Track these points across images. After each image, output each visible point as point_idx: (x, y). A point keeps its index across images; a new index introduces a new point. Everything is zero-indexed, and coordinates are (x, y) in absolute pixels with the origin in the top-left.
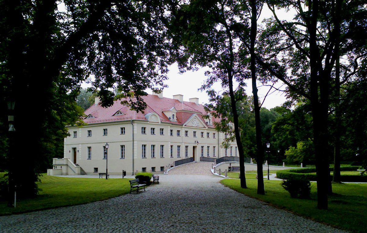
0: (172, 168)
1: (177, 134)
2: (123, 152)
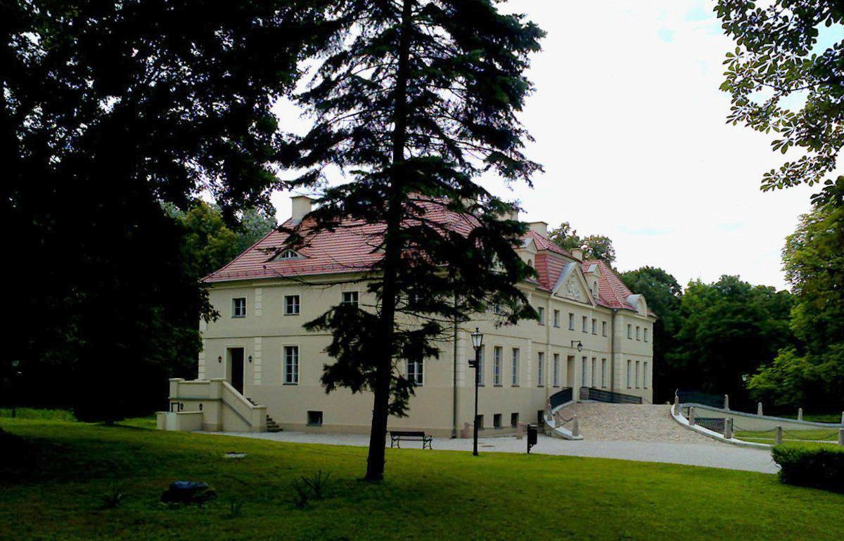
2: (293, 364)
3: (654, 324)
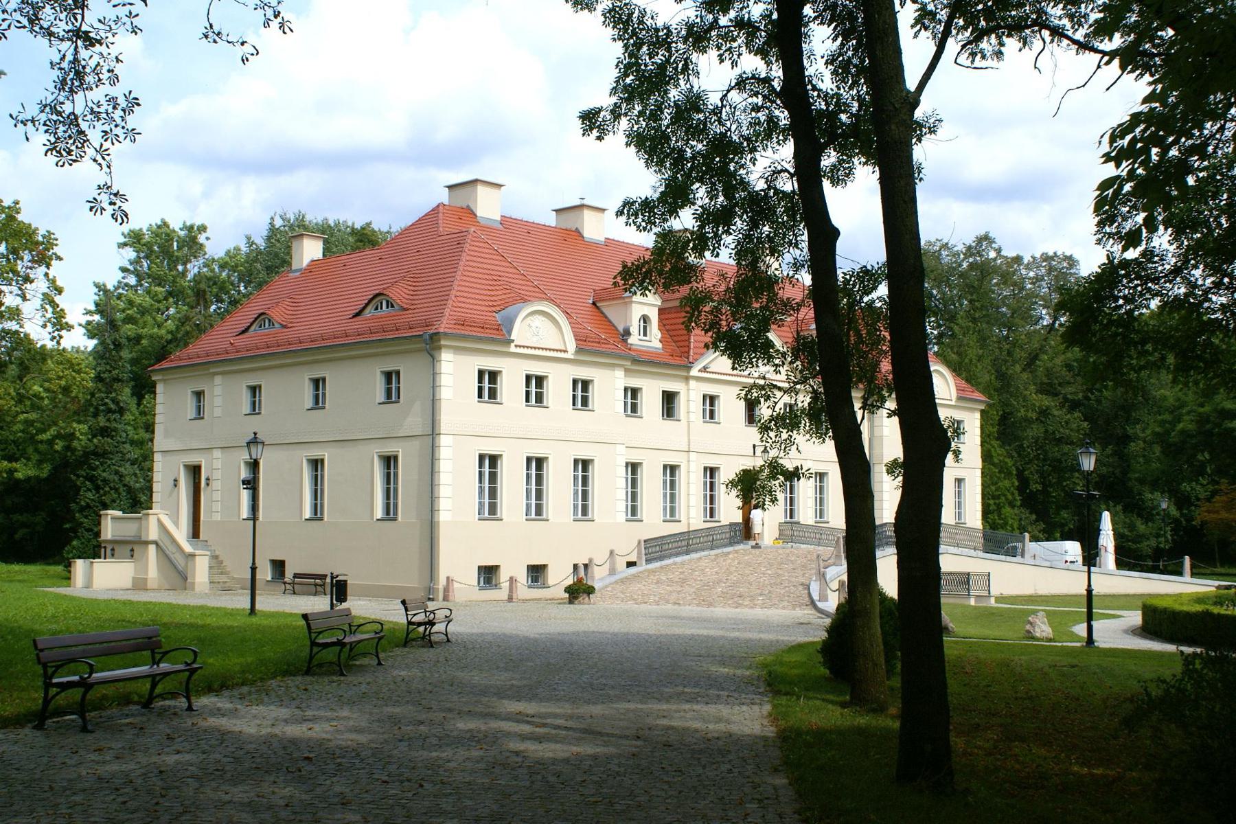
0: (633, 570)
1: (704, 410)
3: (982, 412)
